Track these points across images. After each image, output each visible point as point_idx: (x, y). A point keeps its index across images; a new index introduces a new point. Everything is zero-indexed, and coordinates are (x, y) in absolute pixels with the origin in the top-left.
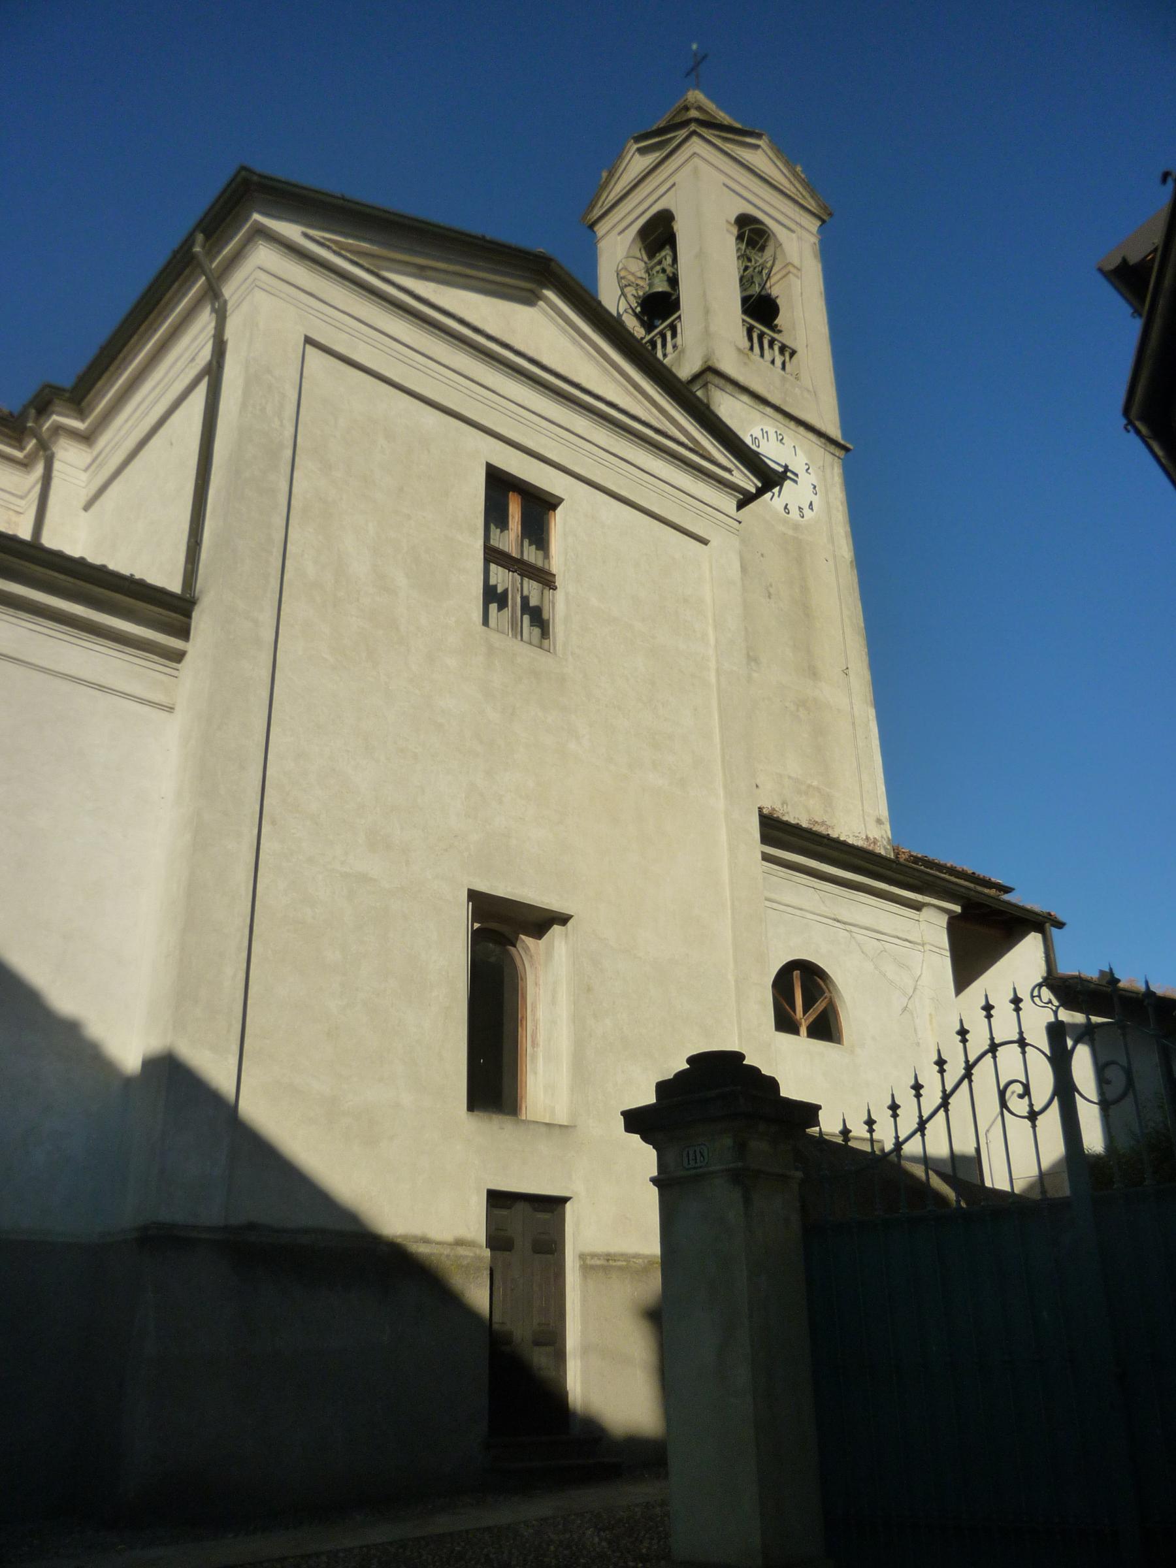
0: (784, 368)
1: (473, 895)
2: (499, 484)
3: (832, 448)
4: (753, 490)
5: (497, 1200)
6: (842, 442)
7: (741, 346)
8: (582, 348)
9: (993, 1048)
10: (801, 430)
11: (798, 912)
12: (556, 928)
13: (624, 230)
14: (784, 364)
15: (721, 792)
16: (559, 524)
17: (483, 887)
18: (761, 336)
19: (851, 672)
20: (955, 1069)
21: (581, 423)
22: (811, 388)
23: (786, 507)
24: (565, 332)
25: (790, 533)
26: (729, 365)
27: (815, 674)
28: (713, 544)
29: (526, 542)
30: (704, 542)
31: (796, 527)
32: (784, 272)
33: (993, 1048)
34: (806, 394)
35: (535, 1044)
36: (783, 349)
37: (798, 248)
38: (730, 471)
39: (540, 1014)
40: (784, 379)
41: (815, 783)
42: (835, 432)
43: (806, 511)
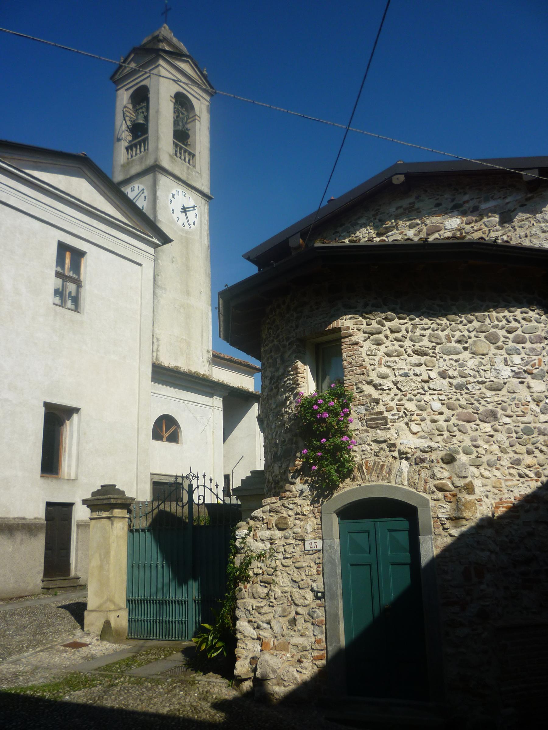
1: (46, 405)
2: (63, 248)
5: (49, 505)
6: (210, 195)
9: (198, 487)
14: (189, 161)
17: (49, 400)
19: (203, 293)
23: (183, 224)
25: (184, 235)
26: (165, 163)
27: (188, 294)
28: (143, 265)
30: (140, 265)
31: (187, 232)
33: (198, 487)
34: (197, 175)
35: (65, 451)
36: (190, 154)
37: (201, 105)
40: (188, 168)
41: (184, 338)
42: (206, 189)
43: (192, 225)
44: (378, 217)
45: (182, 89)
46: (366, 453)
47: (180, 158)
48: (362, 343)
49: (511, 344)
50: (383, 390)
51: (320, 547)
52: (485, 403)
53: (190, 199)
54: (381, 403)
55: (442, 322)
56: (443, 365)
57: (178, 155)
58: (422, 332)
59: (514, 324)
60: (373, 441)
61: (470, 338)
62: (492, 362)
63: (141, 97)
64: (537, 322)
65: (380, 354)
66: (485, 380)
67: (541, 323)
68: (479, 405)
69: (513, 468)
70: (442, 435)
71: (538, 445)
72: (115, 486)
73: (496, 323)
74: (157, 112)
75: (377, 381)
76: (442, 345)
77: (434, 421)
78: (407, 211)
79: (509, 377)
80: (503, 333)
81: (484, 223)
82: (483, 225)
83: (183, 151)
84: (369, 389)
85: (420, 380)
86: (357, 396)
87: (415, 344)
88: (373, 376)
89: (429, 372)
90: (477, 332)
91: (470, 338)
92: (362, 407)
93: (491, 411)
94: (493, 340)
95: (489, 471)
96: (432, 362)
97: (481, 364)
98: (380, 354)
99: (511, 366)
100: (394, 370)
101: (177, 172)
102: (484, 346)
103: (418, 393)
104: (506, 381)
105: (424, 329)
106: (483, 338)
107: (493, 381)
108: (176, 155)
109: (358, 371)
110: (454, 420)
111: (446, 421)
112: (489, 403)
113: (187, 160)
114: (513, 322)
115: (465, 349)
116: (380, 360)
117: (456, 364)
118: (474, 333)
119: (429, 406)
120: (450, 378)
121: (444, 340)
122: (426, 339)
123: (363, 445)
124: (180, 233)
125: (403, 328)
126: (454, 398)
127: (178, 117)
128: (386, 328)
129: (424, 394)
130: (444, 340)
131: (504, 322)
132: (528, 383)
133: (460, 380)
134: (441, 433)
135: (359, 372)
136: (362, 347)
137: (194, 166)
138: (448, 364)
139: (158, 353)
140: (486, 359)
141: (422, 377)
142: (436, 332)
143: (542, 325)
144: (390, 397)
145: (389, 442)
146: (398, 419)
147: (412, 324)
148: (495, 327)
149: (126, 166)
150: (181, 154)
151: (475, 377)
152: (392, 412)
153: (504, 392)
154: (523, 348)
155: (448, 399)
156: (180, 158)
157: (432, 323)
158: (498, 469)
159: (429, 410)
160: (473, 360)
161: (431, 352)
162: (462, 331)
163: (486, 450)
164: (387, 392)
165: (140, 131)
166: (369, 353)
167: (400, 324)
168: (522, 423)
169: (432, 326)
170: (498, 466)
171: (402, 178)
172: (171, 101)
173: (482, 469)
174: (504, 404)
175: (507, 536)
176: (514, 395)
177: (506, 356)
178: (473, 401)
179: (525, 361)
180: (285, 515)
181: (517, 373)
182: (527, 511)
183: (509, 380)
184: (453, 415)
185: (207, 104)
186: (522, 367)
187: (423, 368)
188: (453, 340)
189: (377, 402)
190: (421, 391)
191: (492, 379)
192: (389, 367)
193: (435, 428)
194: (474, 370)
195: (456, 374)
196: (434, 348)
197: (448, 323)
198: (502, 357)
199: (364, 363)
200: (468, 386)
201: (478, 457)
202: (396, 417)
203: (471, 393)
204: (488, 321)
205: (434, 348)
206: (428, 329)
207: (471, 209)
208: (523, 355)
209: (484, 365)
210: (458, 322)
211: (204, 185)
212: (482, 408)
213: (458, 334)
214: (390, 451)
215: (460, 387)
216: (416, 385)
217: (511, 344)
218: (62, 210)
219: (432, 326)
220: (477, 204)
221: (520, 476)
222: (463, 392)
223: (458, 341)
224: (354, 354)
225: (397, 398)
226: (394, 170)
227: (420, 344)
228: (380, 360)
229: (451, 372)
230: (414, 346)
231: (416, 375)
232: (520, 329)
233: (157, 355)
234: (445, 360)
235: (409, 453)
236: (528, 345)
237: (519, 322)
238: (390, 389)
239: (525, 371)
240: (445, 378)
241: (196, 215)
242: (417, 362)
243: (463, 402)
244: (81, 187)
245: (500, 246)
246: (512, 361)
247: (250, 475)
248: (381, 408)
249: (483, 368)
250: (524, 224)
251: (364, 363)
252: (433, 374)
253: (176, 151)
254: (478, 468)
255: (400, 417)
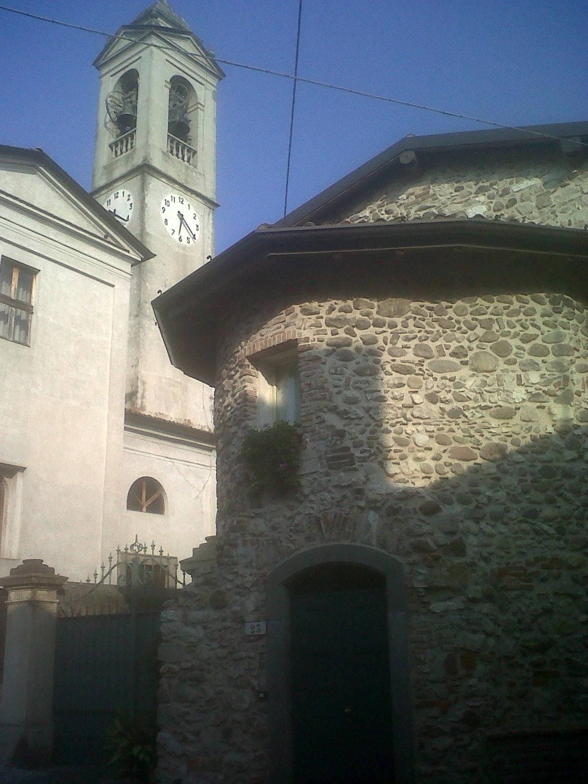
0: (188, 161)
3: (209, 205)
4: (140, 260)
7: (165, 150)
8: (57, 192)
10: (194, 196)
11: (147, 455)
12: (19, 474)
13: (114, 74)
15: (107, 406)
16: (38, 283)
18: (178, 144)
20: (107, 570)
21: (52, 232)
22: (202, 173)
24: (49, 185)
25: (181, 251)
26: (157, 162)
28: (116, 287)
29: (21, 289)
30: (113, 286)
31: (184, 248)
32: (195, 107)
34: (199, 176)
35: (6, 523)
36: (189, 150)
38: (128, 252)
39: (9, 511)
40: (187, 168)
42: (210, 195)
44: (384, 209)
45: (180, 72)
46: (325, 502)
47: (177, 155)
48: (324, 359)
49: (527, 357)
50: (349, 418)
51: (263, 632)
52: (489, 435)
53: (191, 209)
54: (347, 436)
55: (433, 330)
56: (432, 385)
57: (175, 152)
58: (406, 343)
59: (532, 331)
60: (336, 487)
61: (471, 349)
62: (499, 380)
63: (130, 82)
64: (564, 328)
65: (348, 372)
66: (490, 405)
67: (569, 329)
68: (480, 438)
69: (527, 522)
70: (429, 478)
71: (562, 491)
72: (42, 561)
73: (507, 329)
74: (148, 100)
75: (343, 407)
76: (432, 360)
77: (417, 459)
78: (420, 199)
79: (524, 400)
80: (514, 342)
81: (516, 209)
82: (515, 210)
83: (186, 150)
84: (332, 419)
85: (401, 406)
86: (317, 428)
87: (395, 358)
88: (339, 401)
89: (413, 395)
90: (480, 341)
91: (471, 349)
92: (323, 442)
93: (497, 445)
94: (502, 350)
95: (493, 526)
96: (416, 381)
97: (484, 383)
98: (348, 372)
99: (526, 386)
100: (365, 392)
101: (172, 173)
102: (490, 358)
103: (397, 423)
104: (519, 405)
105: (408, 339)
106: (488, 350)
107: (500, 406)
108: (172, 152)
109: (319, 395)
110: (445, 458)
111: (434, 459)
112: (494, 434)
113: (186, 158)
114: (531, 327)
115: (465, 363)
116: (348, 379)
117: (451, 384)
118: (477, 342)
119: (411, 440)
120: (442, 402)
121: (435, 353)
122: (410, 352)
123: (322, 493)
124: (177, 250)
125: (380, 338)
126: (447, 428)
127: (175, 105)
128: (358, 338)
129: (406, 424)
130: (435, 353)
131: (519, 328)
132: (549, 409)
133: (455, 404)
134: (428, 475)
135: (320, 397)
136: (324, 363)
137: (195, 167)
138: (439, 384)
139: (144, 400)
140: (492, 377)
141: (403, 402)
142: (425, 342)
143: (571, 331)
144: (359, 428)
145: (356, 487)
146: (370, 456)
147: (391, 333)
148: (507, 334)
149: (109, 168)
150: (178, 150)
151: (476, 400)
152: (361, 449)
153: (516, 420)
154: (543, 362)
155: (439, 430)
156: (177, 155)
157: (420, 332)
158: (505, 524)
159: (412, 445)
160: (473, 379)
161: (417, 368)
162: (460, 340)
163: (489, 498)
164: (356, 421)
165: (126, 123)
166: (333, 371)
167: (376, 333)
168: (540, 462)
169: (419, 335)
170: (505, 520)
171: (412, 155)
172: (165, 86)
173: (483, 524)
174: (515, 436)
175: (514, 614)
176: (530, 424)
177: (520, 372)
178: (472, 432)
179: (546, 379)
180: (223, 589)
181: (534, 396)
182: (544, 580)
183: (524, 404)
184: (445, 451)
185: (214, 89)
186: (541, 387)
187: (405, 390)
188: (447, 352)
189: (341, 434)
190: (402, 419)
191: (500, 403)
192: (360, 388)
193: (419, 469)
194: (476, 392)
195: (449, 396)
196: (421, 363)
197: (441, 330)
198: (515, 374)
199: (326, 385)
200: (466, 413)
201: (477, 507)
202: (367, 454)
203: (470, 422)
204: (495, 327)
205: (421, 363)
206: (414, 338)
207: (500, 193)
208: (543, 371)
209: (489, 386)
210: (455, 329)
211: (208, 187)
212: (484, 443)
213: (454, 345)
214: (357, 499)
215: (455, 414)
216: (395, 412)
217: (527, 357)
218: (8, 218)
219: (419, 335)
220: (507, 186)
221: (537, 533)
222: (459, 421)
223: (454, 354)
224: (314, 373)
225: (369, 429)
226: (403, 146)
227: (402, 358)
228: (348, 379)
229: (442, 395)
230: (394, 361)
231: (394, 398)
232: (540, 337)
233: (142, 403)
234: (436, 379)
235: (379, 502)
236: (551, 358)
237: (539, 328)
238: (360, 418)
239: (544, 391)
240: (435, 403)
241: (197, 226)
242: (396, 382)
243: (459, 434)
244: (35, 188)
245: (504, 225)
246: (528, 380)
247: (206, 542)
248: (348, 443)
249: (487, 388)
250: (567, 209)
251: (326, 385)
252: (418, 398)
253: (172, 148)
254: (477, 523)
255: (371, 455)
